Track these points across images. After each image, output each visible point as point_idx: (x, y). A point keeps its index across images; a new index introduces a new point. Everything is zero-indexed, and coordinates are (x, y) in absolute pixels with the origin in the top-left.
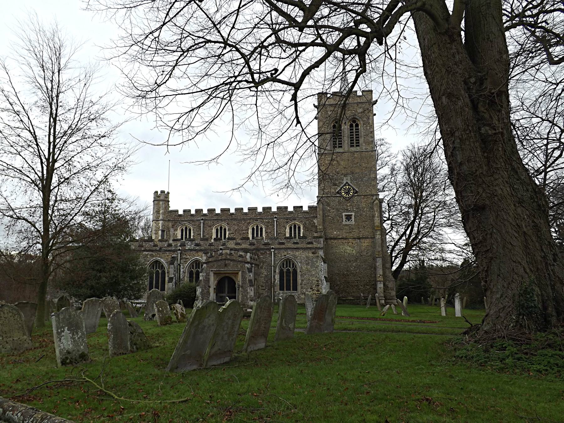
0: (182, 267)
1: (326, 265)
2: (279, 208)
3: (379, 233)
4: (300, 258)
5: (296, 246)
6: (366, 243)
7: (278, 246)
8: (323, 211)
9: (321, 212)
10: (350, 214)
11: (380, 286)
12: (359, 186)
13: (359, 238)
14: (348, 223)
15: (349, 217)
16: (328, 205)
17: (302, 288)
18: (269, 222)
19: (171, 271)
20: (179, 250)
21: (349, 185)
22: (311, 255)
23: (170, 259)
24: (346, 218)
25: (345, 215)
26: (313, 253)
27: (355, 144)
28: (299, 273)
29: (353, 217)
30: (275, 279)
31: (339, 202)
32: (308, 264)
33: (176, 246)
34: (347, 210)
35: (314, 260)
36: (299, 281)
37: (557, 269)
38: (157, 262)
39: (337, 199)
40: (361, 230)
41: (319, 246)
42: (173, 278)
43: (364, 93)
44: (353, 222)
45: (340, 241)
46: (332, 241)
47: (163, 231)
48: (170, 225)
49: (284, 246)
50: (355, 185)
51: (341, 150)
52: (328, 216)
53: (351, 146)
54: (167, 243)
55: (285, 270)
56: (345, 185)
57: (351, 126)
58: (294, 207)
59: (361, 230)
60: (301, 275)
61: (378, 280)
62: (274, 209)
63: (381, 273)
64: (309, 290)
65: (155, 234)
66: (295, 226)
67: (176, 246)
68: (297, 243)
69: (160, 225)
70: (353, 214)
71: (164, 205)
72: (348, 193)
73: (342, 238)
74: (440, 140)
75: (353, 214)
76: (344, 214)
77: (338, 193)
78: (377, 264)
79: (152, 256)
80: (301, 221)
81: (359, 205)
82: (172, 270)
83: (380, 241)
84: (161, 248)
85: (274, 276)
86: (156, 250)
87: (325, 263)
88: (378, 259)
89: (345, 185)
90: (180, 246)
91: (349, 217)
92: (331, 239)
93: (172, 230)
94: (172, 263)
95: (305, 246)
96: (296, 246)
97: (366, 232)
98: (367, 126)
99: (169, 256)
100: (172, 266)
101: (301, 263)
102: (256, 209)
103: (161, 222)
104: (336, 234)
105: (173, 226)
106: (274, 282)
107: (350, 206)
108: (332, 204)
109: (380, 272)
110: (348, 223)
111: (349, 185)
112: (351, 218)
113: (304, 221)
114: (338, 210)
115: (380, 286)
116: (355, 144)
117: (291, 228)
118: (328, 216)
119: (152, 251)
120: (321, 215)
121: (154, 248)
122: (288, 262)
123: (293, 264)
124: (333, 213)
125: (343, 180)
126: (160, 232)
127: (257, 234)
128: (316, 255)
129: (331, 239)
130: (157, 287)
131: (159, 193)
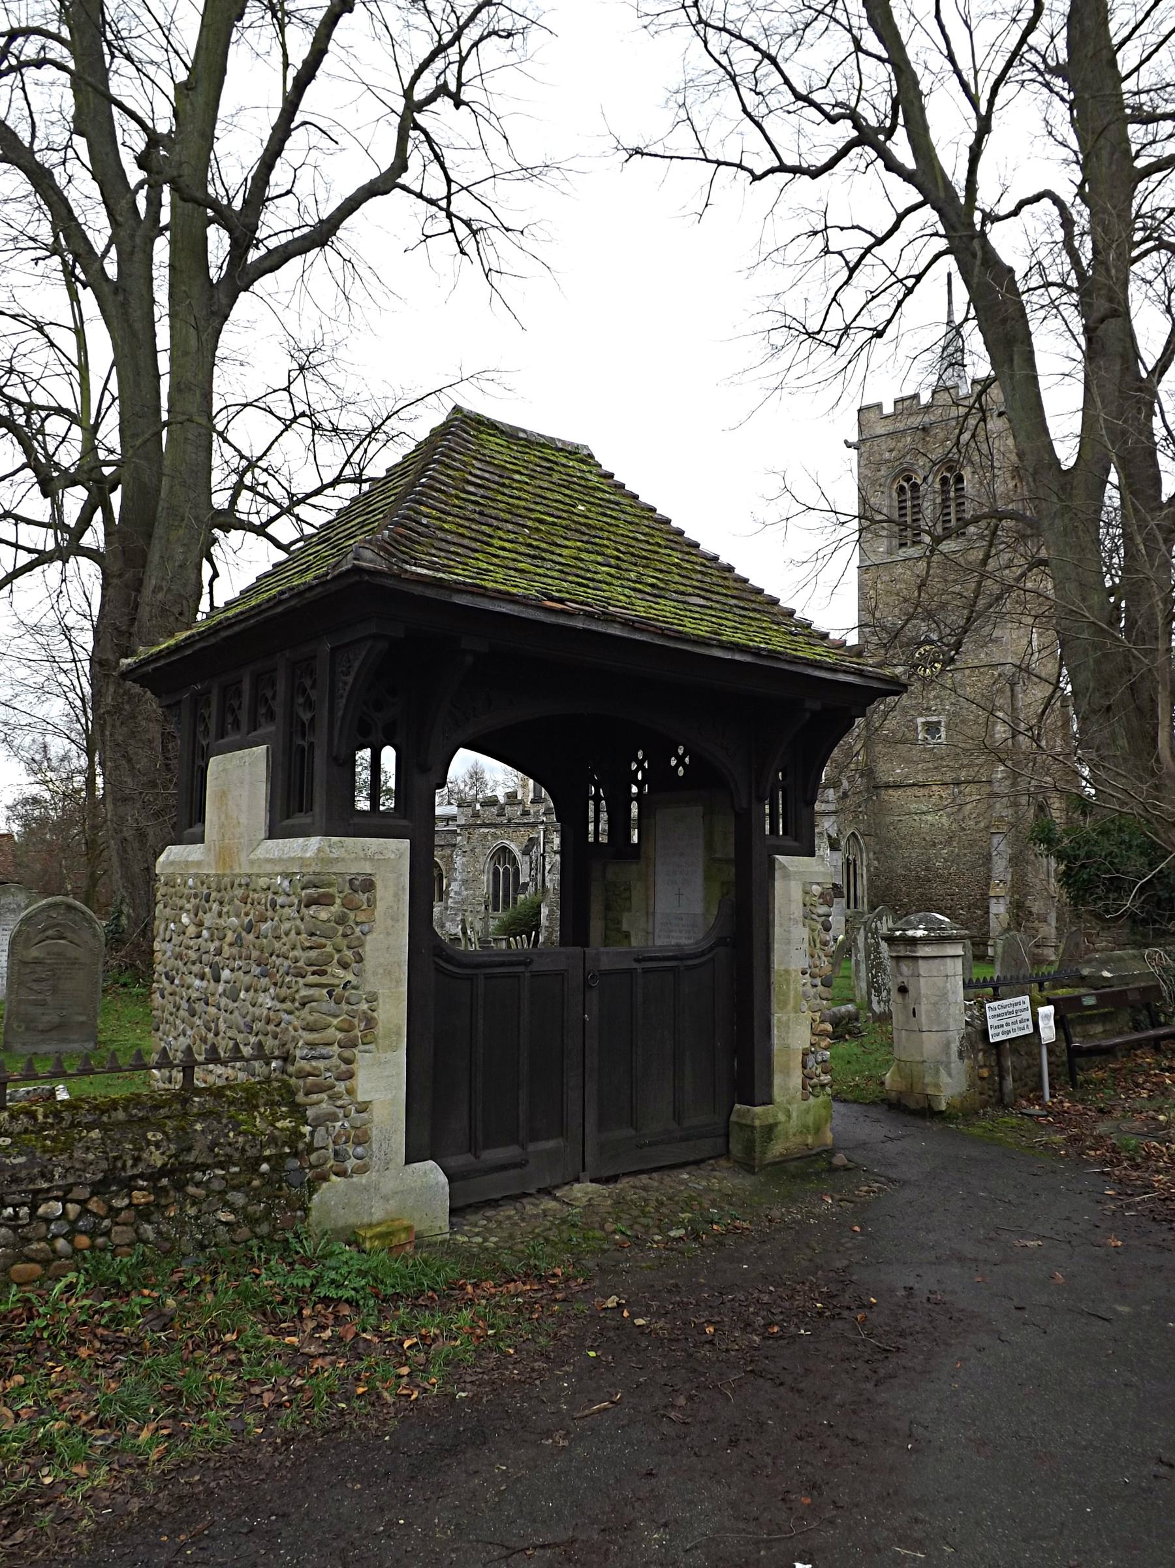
0: (547, 859)
10: (934, 719)
20: (542, 822)
23: (526, 842)
25: (939, 722)
33: (537, 814)
34: (928, 709)
38: (505, 850)
42: (527, 884)
45: (909, 791)
46: (891, 792)
54: (521, 807)
57: (944, 481)
61: (991, 893)
67: (537, 814)
73: (913, 785)
74: (29, 394)
75: (943, 719)
86: (502, 824)
90: (544, 814)
91: (932, 728)
92: (888, 786)
99: (524, 834)
100: (527, 858)
104: (899, 775)
107: (935, 698)
112: (938, 731)
119: (494, 825)
129: (888, 786)
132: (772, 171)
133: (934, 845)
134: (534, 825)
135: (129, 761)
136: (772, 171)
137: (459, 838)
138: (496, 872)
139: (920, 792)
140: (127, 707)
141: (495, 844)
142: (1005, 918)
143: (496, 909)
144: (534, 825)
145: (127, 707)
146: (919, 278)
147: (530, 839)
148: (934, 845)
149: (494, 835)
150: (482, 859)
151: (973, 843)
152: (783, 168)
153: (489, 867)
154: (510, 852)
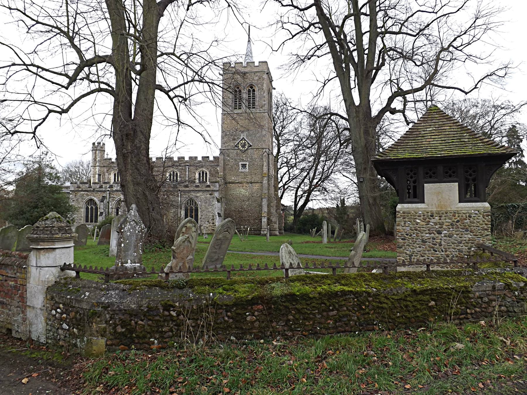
1: (219, 204)
2: (190, 158)
3: (265, 179)
4: (201, 198)
5: (197, 189)
6: (256, 186)
7: (184, 189)
8: (224, 160)
9: (222, 162)
11: (264, 220)
12: (252, 141)
13: (251, 183)
14: (243, 170)
15: (244, 166)
16: (228, 156)
17: (201, 221)
18: (182, 169)
19: (101, 207)
20: (108, 191)
21: (245, 140)
22: (208, 196)
23: (101, 198)
24: (242, 167)
26: (210, 194)
27: (238, 107)
28: (199, 210)
29: (247, 166)
30: (181, 214)
31: (237, 154)
32: (206, 203)
33: (106, 188)
34: (243, 160)
35: (211, 200)
36: (199, 216)
37: (153, 214)
38: (91, 200)
39: (235, 151)
40: (253, 176)
41: (215, 189)
43: (237, 65)
44: (241, 169)
45: (236, 185)
47: (99, 175)
48: (105, 170)
49: (188, 189)
50: (250, 140)
51: (239, 111)
52: (228, 165)
53: (235, 108)
55: (189, 208)
56: (242, 140)
57: (249, 91)
58: (202, 157)
59: (253, 176)
60: (201, 212)
62: (187, 159)
63: (266, 210)
64: (207, 223)
65: (93, 177)
66: (203, 172)
67: (106, 188)
68: (209, 186)
69: (97, 170)
70: (247, 163)
71: (100, 154)
72: (243, 146)
75: (247, 163)
76: (240, 163)
77: (236, 146)
78: (263, 203)
79: (87, 195)
80: (208, 169)
81: (252, 156)
82: (102, 206)
83: (267, 185)
84: (94, 189)
85: (180, 212)
86: (90, 191)
87: (218, 202)
88: (264, 200)
89: (242, 140)
91: (244, 166)
92: (230, 183)
93: (107, 174)
94: (102, 201)
95: (205, 189)
96: (197, 189)
97: (256, 178)
98: (261, 92)
100: (102, 203)
101: (200, 202)
102: (183, 158)
103: (97, 168)
105: (107, 171)
106: (180, 216)
108: (231, 155)
109: (265, 209)
110: (243, 170)
111: (245, 140)
113: (210, 168)
114: (235, 160)
115: (264, 220)
116: (238, 107)
117: (200, 174)
118: (228, 165)
119: (87, 191)
120: (222, 164)
121: (89, 189)
122: (191, 200)
123: (195, 203)
124: (232, 162)
125: (240, 136)
126: (97, 176)
127: (203, 178)
128: (213, 196)
129: (230, 183)
130: (192, 217)
131: (96, 144)
132: (290, 5)
133: (244, 201)
134: (105, 191)
135: (138, 170)
136: (290, 5)
137: (71, 195)
138: (87, 208)
139: (240, 185)
140: (136, 151)
141: (88, 198)
142: (266, 222)
143: (92, 221)
144: (105, 191)
145: (136, 151)
146: (321, 46)
147: (103, 197)
148: (244, 201)
149: (87, 195)
150: (81, 203)
151: (255, 201)
152: (292, 5)
153: (84, 206)
154: (94, 201)
